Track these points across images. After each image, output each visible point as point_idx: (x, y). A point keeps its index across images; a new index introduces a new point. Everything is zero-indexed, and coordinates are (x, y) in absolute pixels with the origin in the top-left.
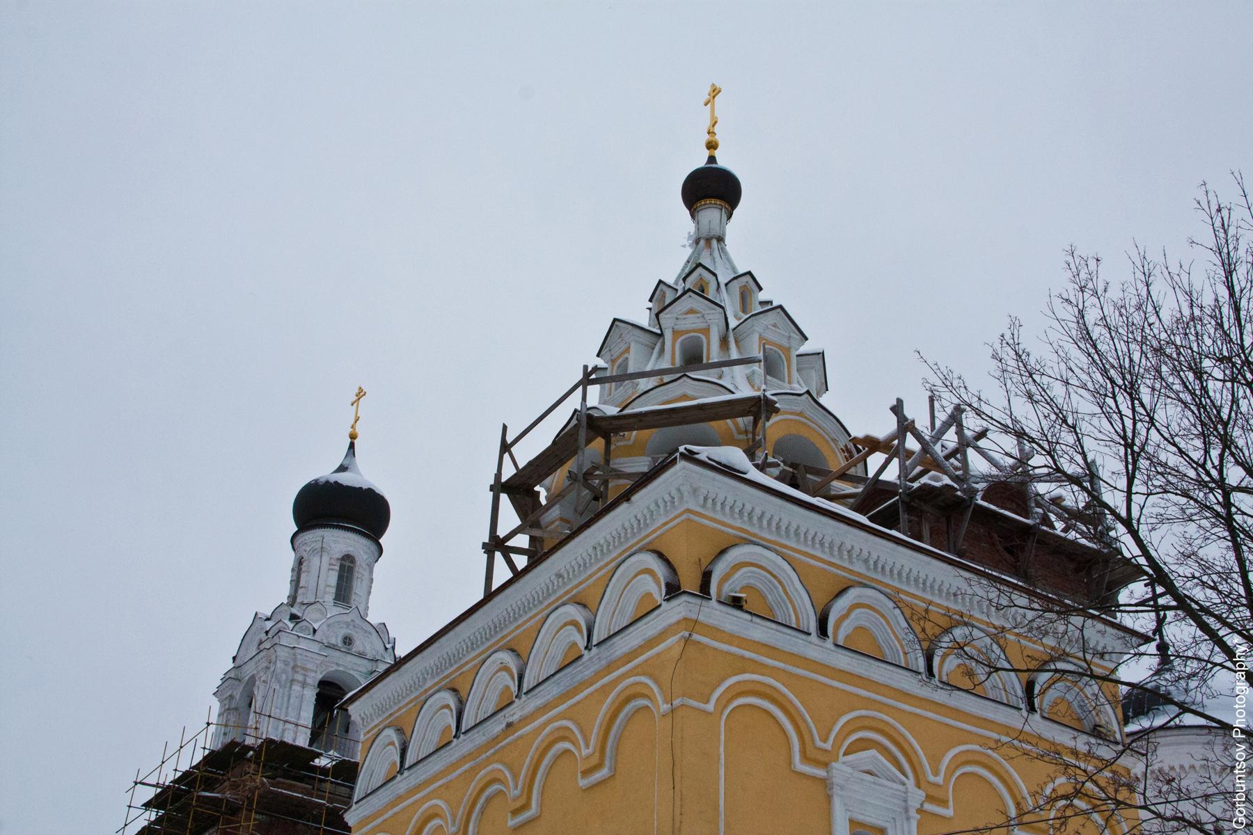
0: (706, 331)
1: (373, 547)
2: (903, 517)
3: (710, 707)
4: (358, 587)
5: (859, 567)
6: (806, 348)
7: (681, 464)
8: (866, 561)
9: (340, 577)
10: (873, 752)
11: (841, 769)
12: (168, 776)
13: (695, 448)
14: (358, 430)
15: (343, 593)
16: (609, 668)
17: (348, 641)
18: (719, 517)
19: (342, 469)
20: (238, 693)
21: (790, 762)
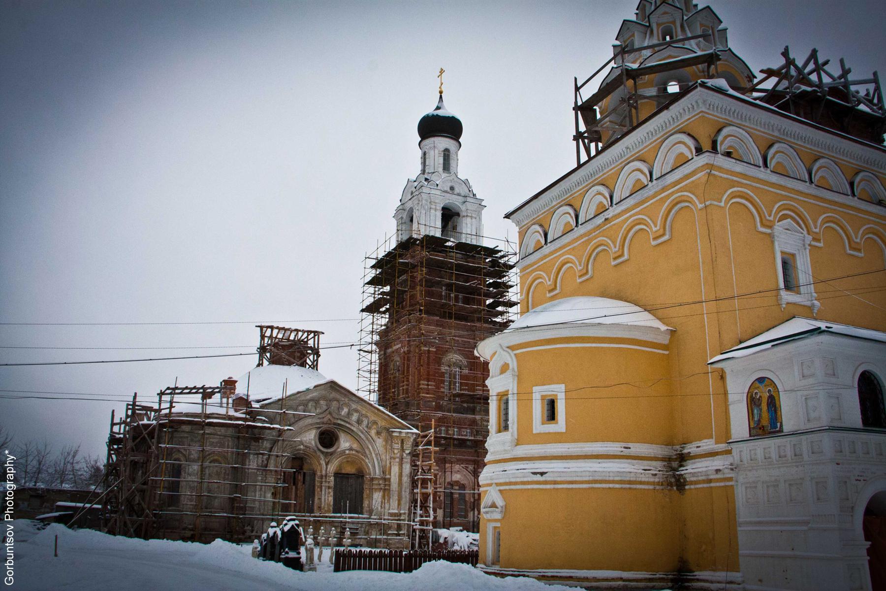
0: (674, 22)
1: (457, 144)
2: (792, 107)
3: (722, 204)
4: (452, 163)
5: (776, 134)
6: (721, 27)
7: (699, 88)
8: (779, 130)
9: (444, 160)
10: (789, 220)
11: (778, 228)
12: (381, 254)
13: (705, 80)
14: (443, 89)
15: (446, 167)
16: (664, 189)
17: (452, 188)
18: (715, 114)
19: (438, 108)
20: (406, 217)
21: (755, 227)
